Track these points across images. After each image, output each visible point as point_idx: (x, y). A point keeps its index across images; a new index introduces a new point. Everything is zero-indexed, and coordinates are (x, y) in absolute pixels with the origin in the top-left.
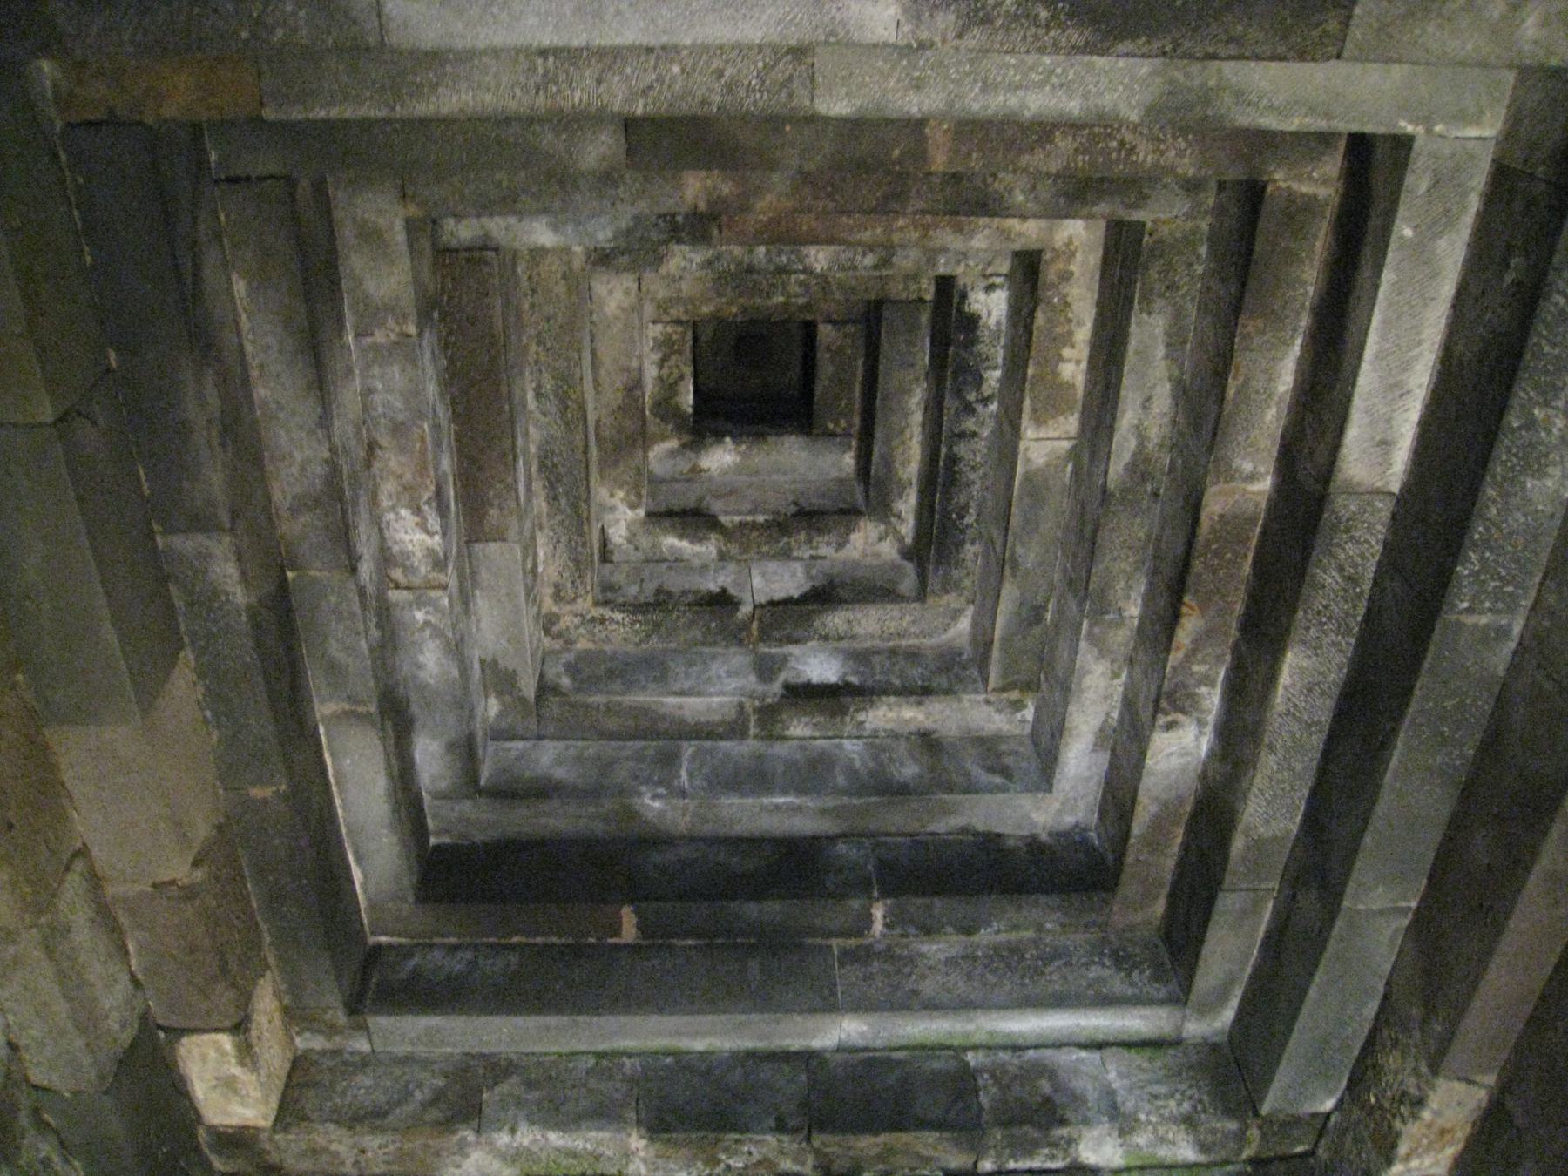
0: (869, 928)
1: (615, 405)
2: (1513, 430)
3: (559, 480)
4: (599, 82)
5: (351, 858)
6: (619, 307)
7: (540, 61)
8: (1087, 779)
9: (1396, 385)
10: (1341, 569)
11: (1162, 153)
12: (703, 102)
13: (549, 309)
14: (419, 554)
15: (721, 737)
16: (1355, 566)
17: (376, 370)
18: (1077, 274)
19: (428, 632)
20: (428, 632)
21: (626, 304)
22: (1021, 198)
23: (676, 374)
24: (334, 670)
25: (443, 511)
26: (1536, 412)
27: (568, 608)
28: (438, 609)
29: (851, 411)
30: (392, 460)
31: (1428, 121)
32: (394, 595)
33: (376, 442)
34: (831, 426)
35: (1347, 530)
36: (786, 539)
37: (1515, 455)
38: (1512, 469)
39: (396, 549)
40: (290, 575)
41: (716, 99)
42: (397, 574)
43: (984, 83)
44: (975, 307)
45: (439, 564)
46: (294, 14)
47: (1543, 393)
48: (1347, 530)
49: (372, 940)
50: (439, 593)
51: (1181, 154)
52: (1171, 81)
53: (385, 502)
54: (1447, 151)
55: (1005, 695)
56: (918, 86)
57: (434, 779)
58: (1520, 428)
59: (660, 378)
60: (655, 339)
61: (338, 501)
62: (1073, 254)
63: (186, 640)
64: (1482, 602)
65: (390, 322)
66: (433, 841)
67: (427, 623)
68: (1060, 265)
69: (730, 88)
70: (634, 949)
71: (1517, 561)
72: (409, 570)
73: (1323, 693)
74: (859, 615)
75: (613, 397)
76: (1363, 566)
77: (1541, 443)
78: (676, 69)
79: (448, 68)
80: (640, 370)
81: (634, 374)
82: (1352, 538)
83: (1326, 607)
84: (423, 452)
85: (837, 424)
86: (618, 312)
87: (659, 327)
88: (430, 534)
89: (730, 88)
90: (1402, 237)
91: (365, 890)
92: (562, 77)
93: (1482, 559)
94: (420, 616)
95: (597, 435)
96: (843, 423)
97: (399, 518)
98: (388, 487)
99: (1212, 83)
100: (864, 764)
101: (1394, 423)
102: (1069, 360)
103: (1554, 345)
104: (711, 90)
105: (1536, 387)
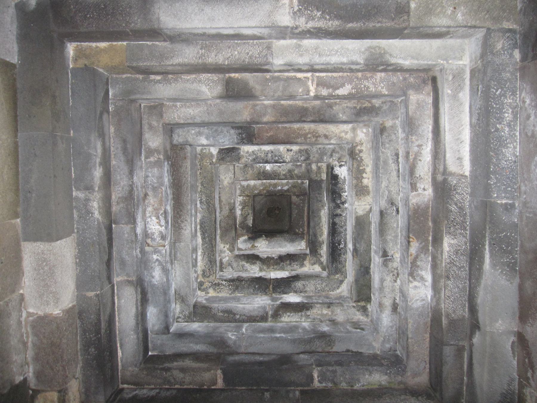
0: (312, 383)
1: (226, 215)
2: (492, 132)
3: (206, 231)
4: (216, 56)
5: (118, 345)
6: (228, 183)
7: (200, 51)
8: (392, 327)
9: (458, 139)
10: (456, 204)
11: (377, 88)
12: (244, 61)
13: (205, 174)
14: (157, 234)
15: (258, 321)
16: (461, 203)
17: (150, 170)
18: (364, 150)
19: (157, 264)
20: (157, 264)
21: (230, 182)
22: (341, 115)
23: (247, 214)
24: (123, 263)
25: (166, 218)
26: (498, 126)
27: (207, 279)
28: (162, 255)
29: (304, 226)
30: (151, 200)
31: (446, 60)
32: (147, 248)
33: (147, 193)
34: (297, 231)
35: (455, 190)
36: (282, 263)
37: (496, 140)
38: (496, 145)
39: (149, 231)
40: (113, 226)
41: (247, 60)
42: (149, 241)
43: (319, 54)
44: (336, 172)
45: (163, 238)
46: (137, 20)
47: (498, 120)
48: (455, 190)
49: (121, 386)
50: (162, 248)
51: (382, 88)
52: (371, 52)
53: (148, 215)
54: (455, 68)
55: (359, 304)
56: (301, 55)
57: (153, 326)
58: (494, 131)
59: (242, 214)
60: (240, 201)
61: (132, 201)
62: (362, 144)
63: (76, 231)
64: (501, 194)
65: (156, 154)
66: (150, 353)
67: (157, 260)
68: (359, 148)
69: (251, 57)
70: (222, 390)
71: (509, 178)
72: (153, 239)
73: (462, 254)
74: (307, 283)
75: (226, 212)
76: (464, 203)
77: (503, 136)
78: (236, 53)
79: (176, 53)
80: (234, 203)
81: (233, 205)
82: (457, 192)
83: (454, 219)
84: (162, 198)
85: (299, 230)
86: (227, 185)
87: (241, 198)
88: (161, 226)
89: (251, 57)
90: (448, 93)
91: (122, 361)
92: (206, 55)
93: (496, 178)
94: (155, 257)
95: (220, 225)
96: (301, 230)
97: (152, 220)
98: (150, 209)
99: (382, 52)
100: (309, 327)
101: (461, 152)
102: (366, 178)
103: (496, 104)
104: (246, 58)
105: (495, 118)
